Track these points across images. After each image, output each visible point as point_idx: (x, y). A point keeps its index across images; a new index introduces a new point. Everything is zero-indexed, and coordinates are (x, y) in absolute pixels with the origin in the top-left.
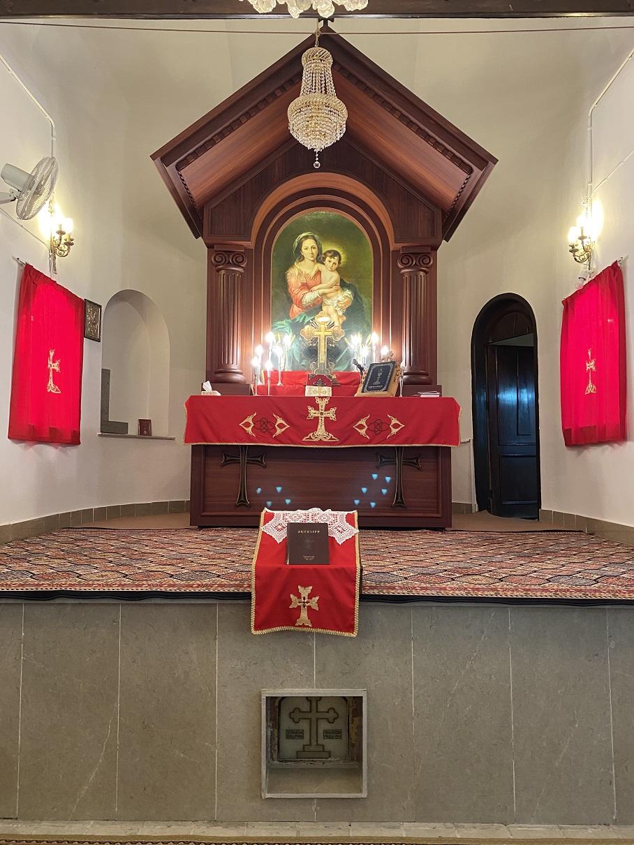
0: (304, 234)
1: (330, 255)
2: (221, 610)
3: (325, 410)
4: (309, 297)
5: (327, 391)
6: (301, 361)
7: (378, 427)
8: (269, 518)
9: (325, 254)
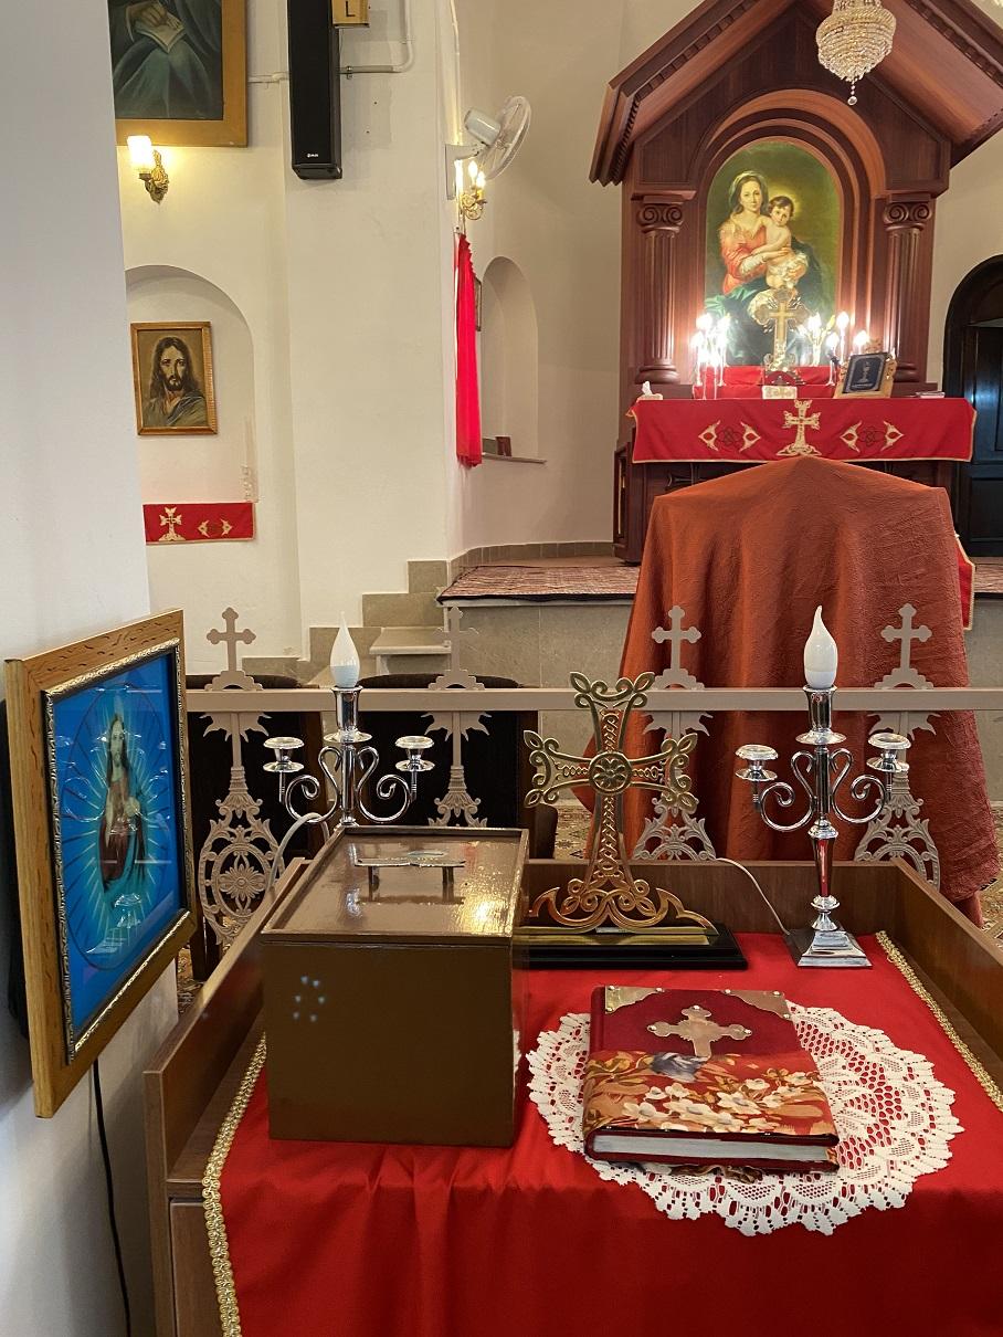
0: (744, 175)
1: (778, 203)
3: (807, 416)
4: (749, 264)
6: (737, 354)
9: (772, 202)
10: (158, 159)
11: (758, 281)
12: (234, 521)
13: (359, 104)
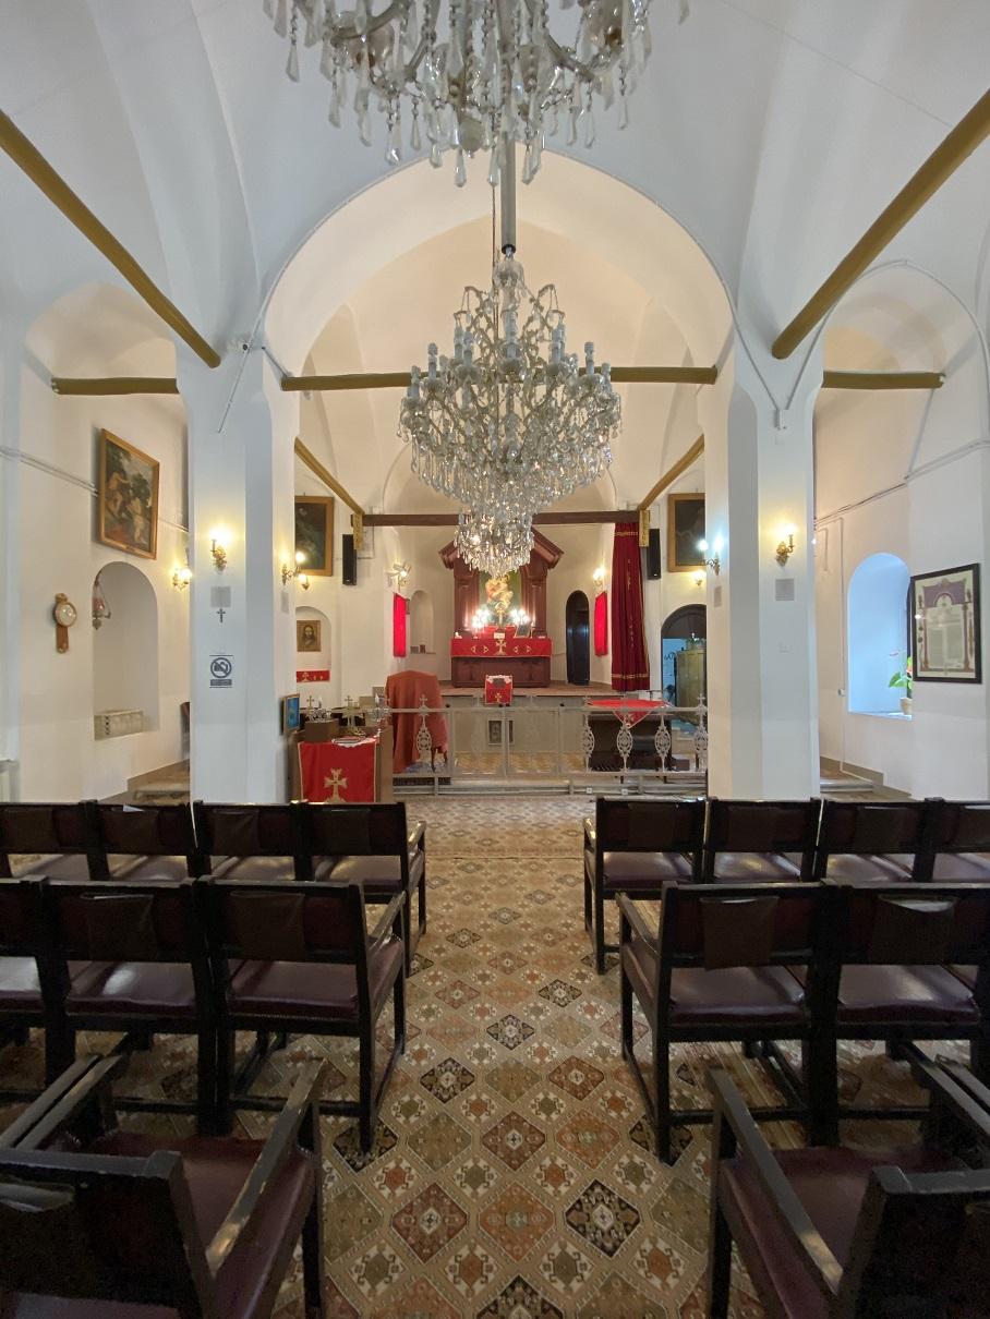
4: (495, 594)
5: (502, 636)
7: (522, 649)
11: (497, 599)
12: (323, 676)
13: (361, 566)
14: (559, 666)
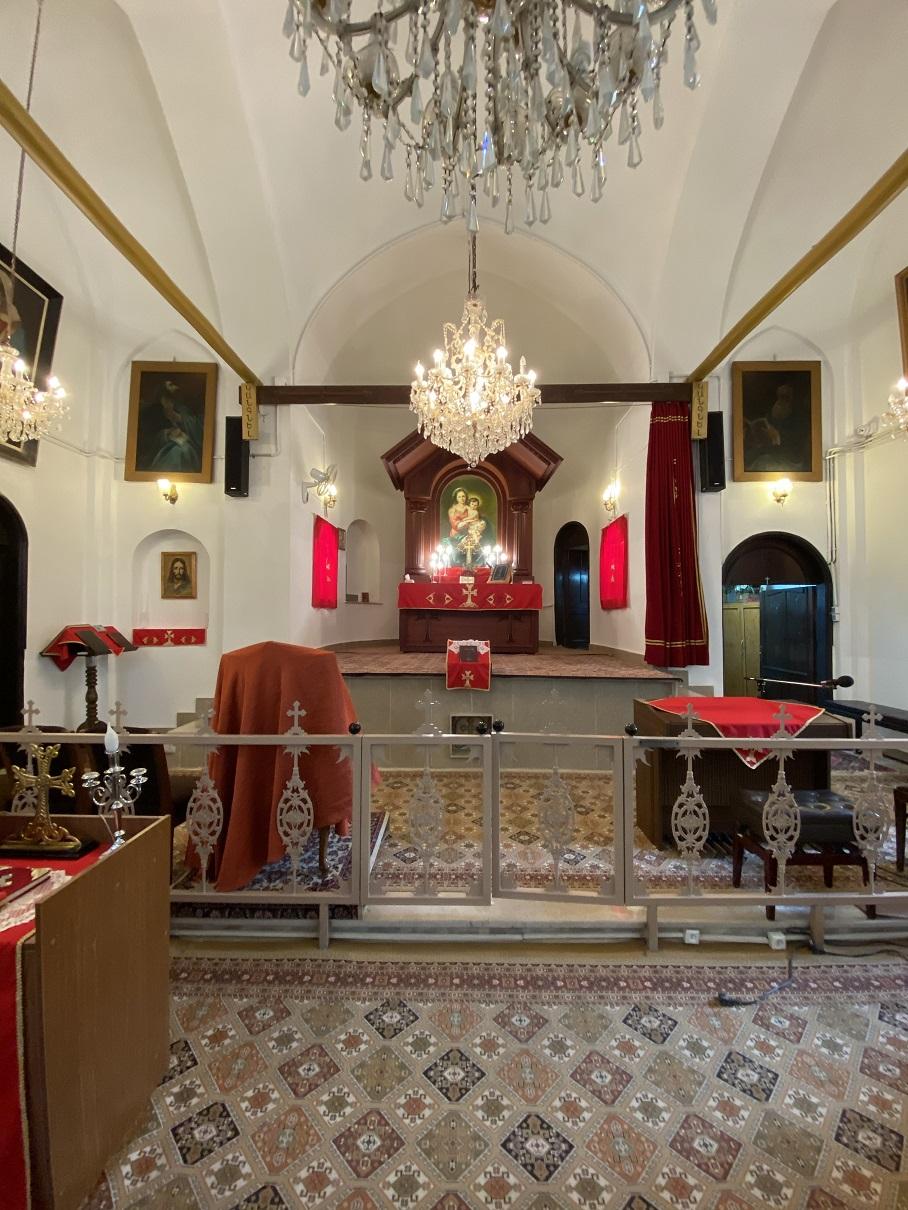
2: (432, 681)
4: (461, 525)
5: (471, 580)
7: (500, 599)
8: (451, 643)
10: (174, 487)
11: (464, 531)
13: (256, 467)
14: (547, 620)
